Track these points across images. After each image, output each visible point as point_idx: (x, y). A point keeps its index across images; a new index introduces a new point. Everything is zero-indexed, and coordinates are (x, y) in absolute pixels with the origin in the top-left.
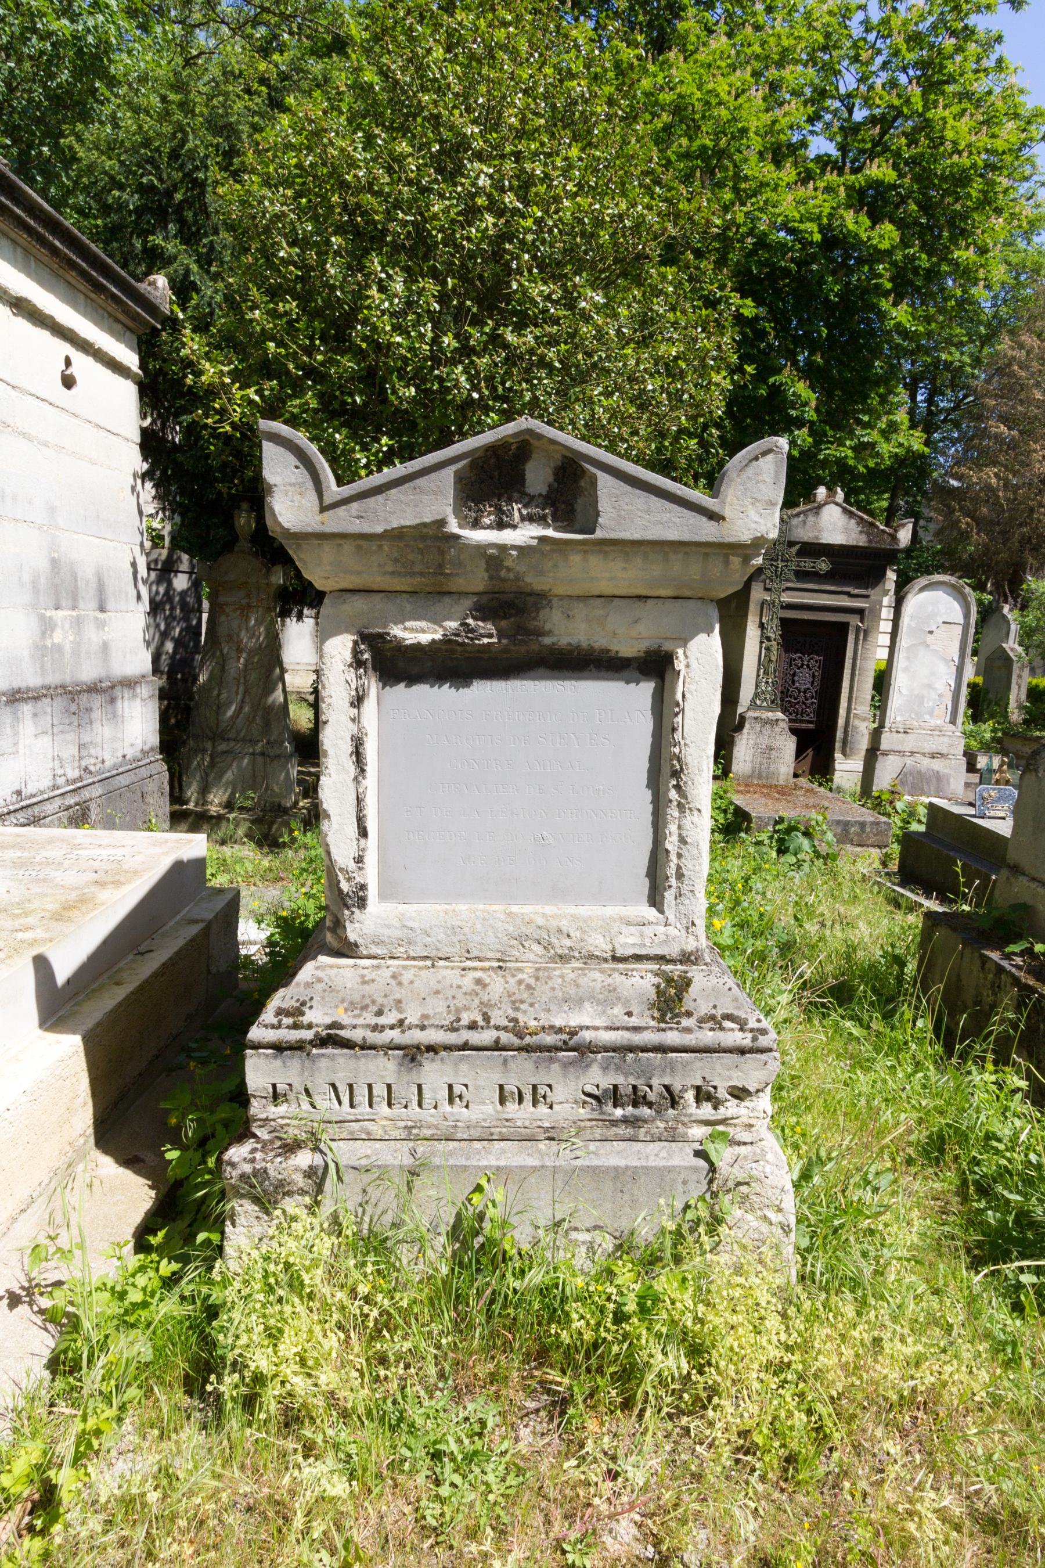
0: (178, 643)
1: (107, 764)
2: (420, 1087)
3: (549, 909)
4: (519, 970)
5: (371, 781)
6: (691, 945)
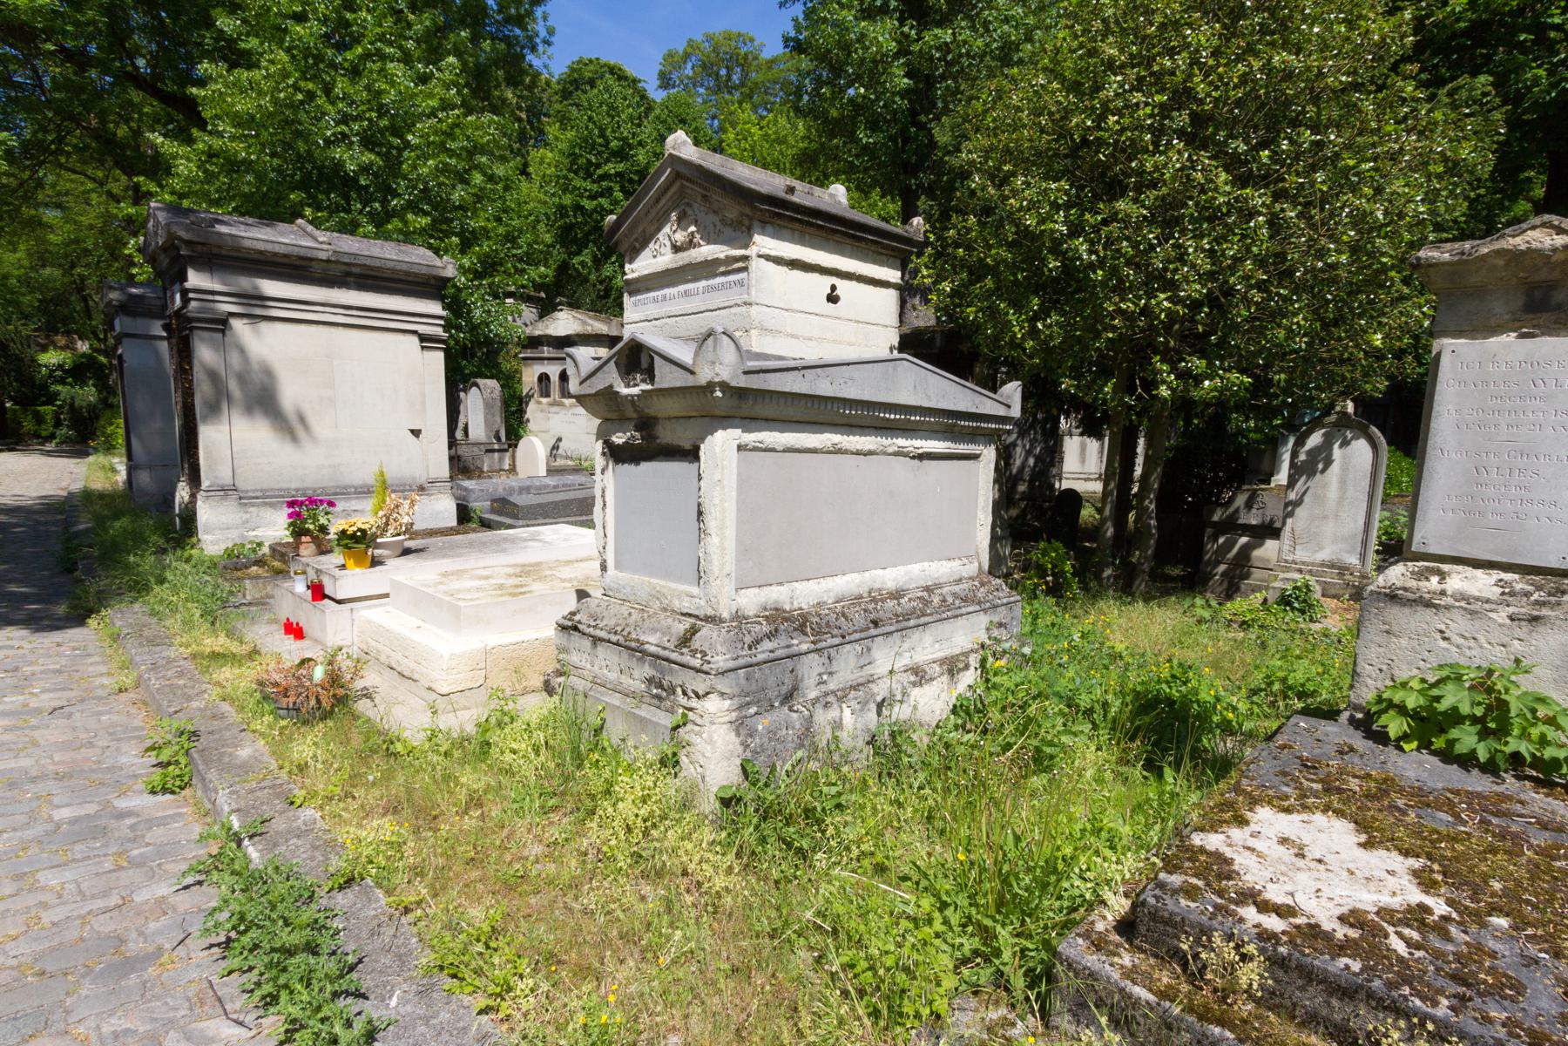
0: (1038, 459)
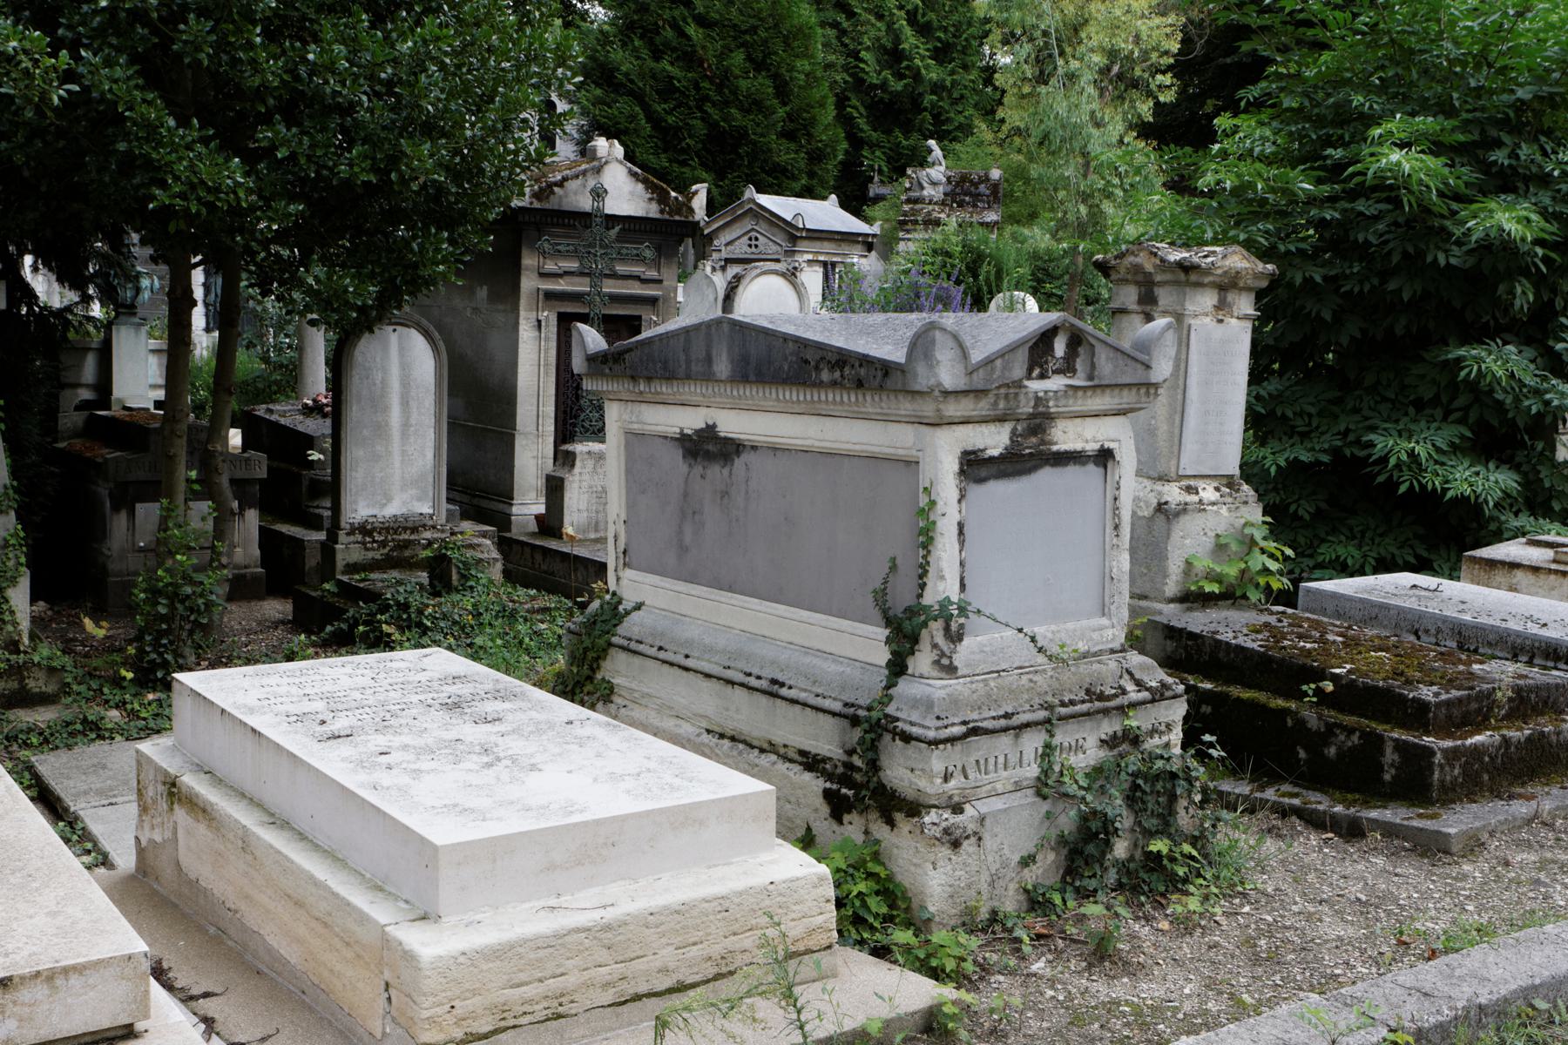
3: (1053, 627)
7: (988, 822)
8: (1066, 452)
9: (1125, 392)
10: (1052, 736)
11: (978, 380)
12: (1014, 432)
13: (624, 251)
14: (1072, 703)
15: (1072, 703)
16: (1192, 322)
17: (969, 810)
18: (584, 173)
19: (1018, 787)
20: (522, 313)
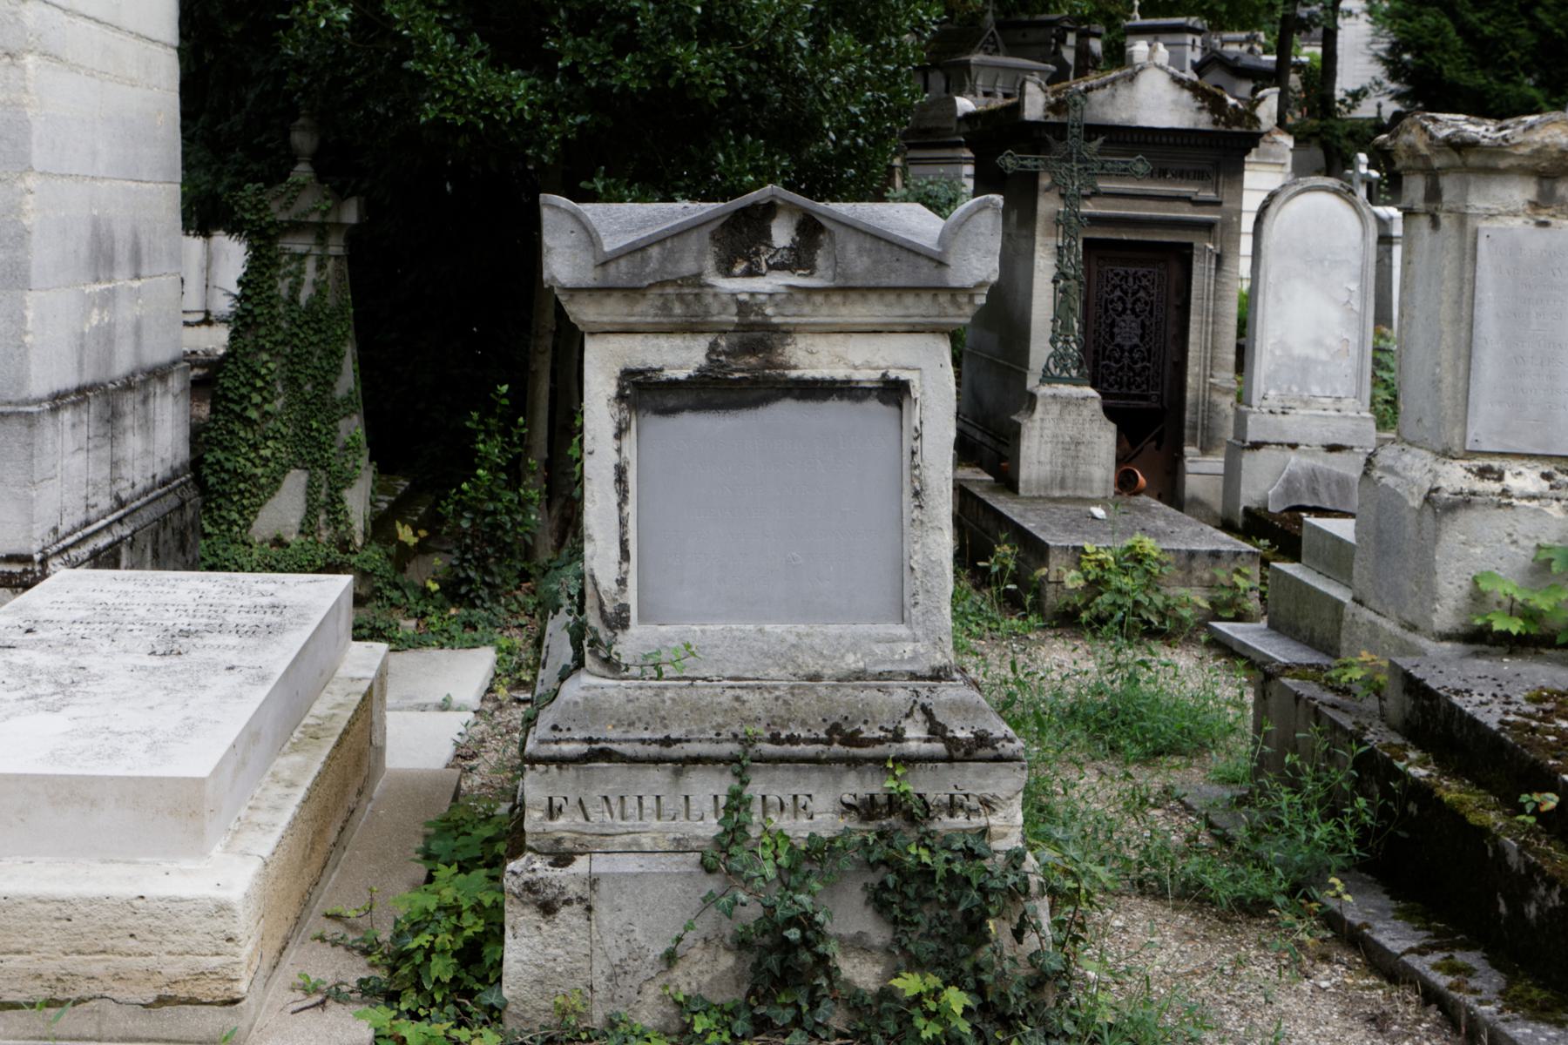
1: (139, 488)
2: (687, 798)
3: (802, 628)
4: (776, 688)
5: (631, 508)
6: (939, 660)
7: (603, 887)
8: (815, 381)
9: (909, 299)
10: (744, 783)
11: (620, 273)
12: (713, 348)
13: (1109, 165)
14: (792, 740)
15: (792, 740)
16: (1483, 224)
17: (580, 865)
18: (1113, 81)
19: (680, 847)
20: (1039, 239)
